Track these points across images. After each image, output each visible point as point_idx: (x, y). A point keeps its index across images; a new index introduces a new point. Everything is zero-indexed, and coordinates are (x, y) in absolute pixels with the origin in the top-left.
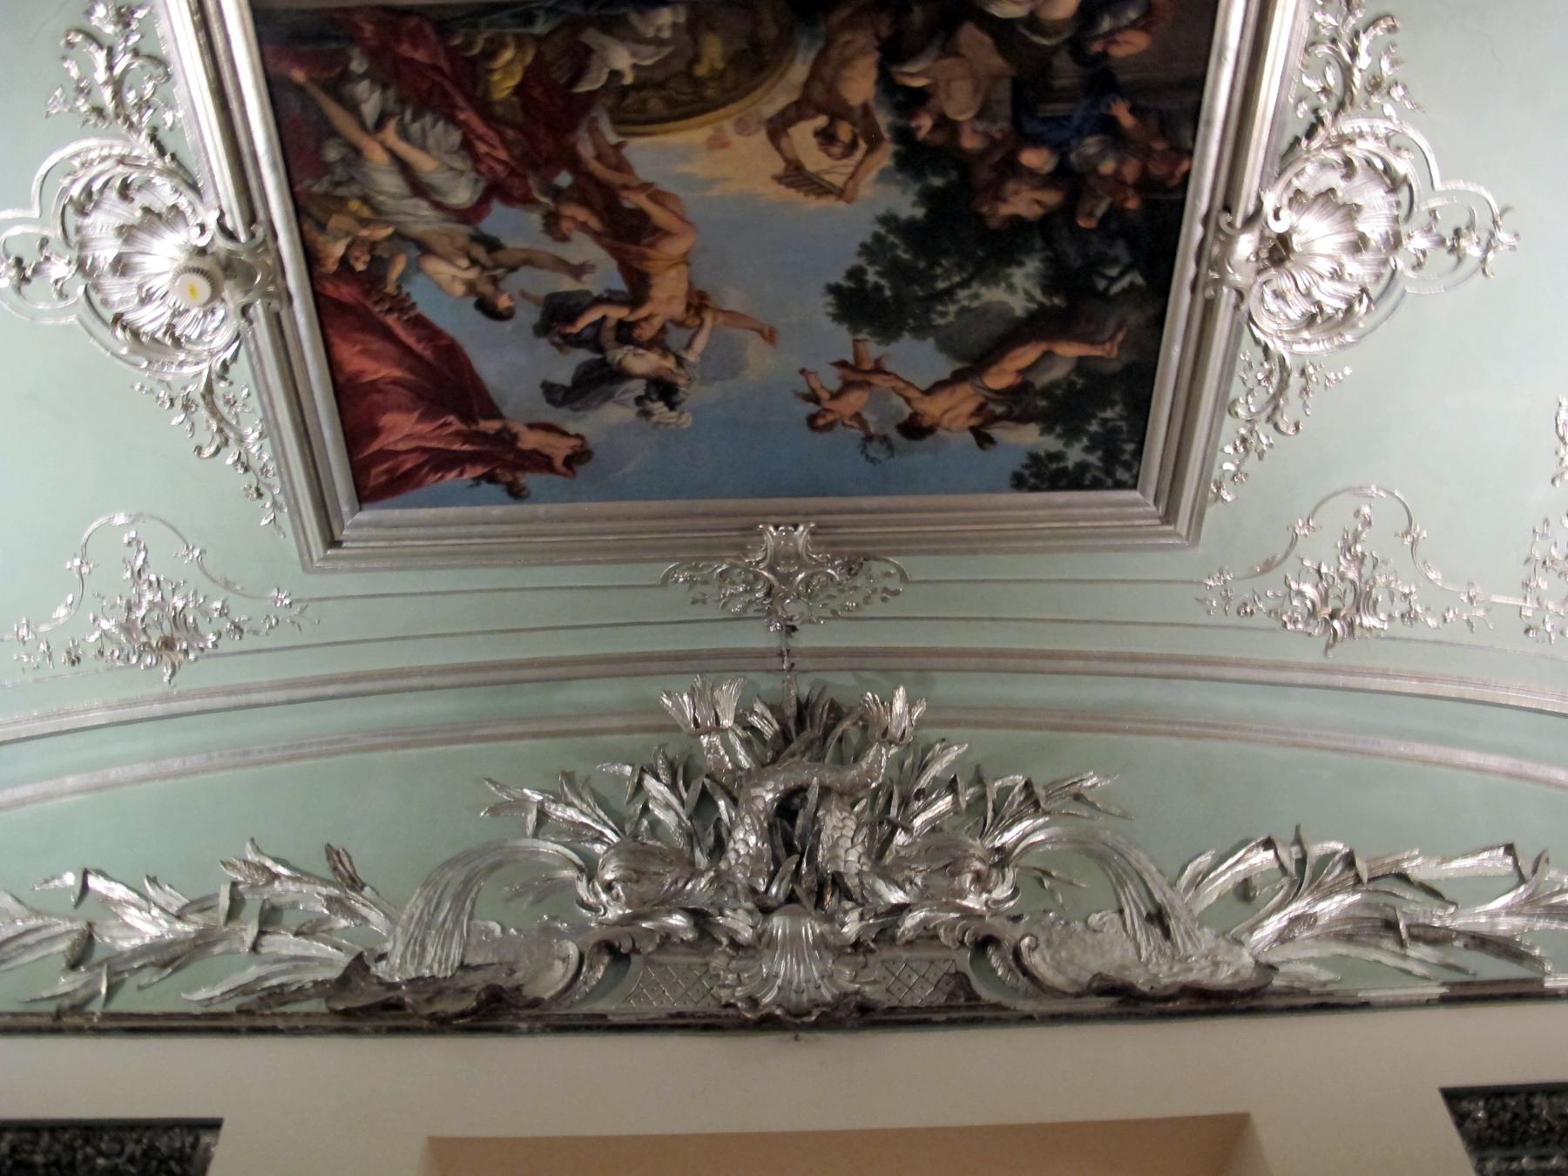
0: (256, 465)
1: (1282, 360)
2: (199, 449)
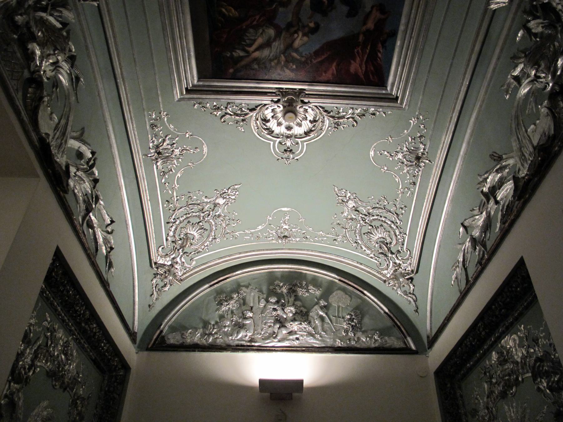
2: (353, 126)
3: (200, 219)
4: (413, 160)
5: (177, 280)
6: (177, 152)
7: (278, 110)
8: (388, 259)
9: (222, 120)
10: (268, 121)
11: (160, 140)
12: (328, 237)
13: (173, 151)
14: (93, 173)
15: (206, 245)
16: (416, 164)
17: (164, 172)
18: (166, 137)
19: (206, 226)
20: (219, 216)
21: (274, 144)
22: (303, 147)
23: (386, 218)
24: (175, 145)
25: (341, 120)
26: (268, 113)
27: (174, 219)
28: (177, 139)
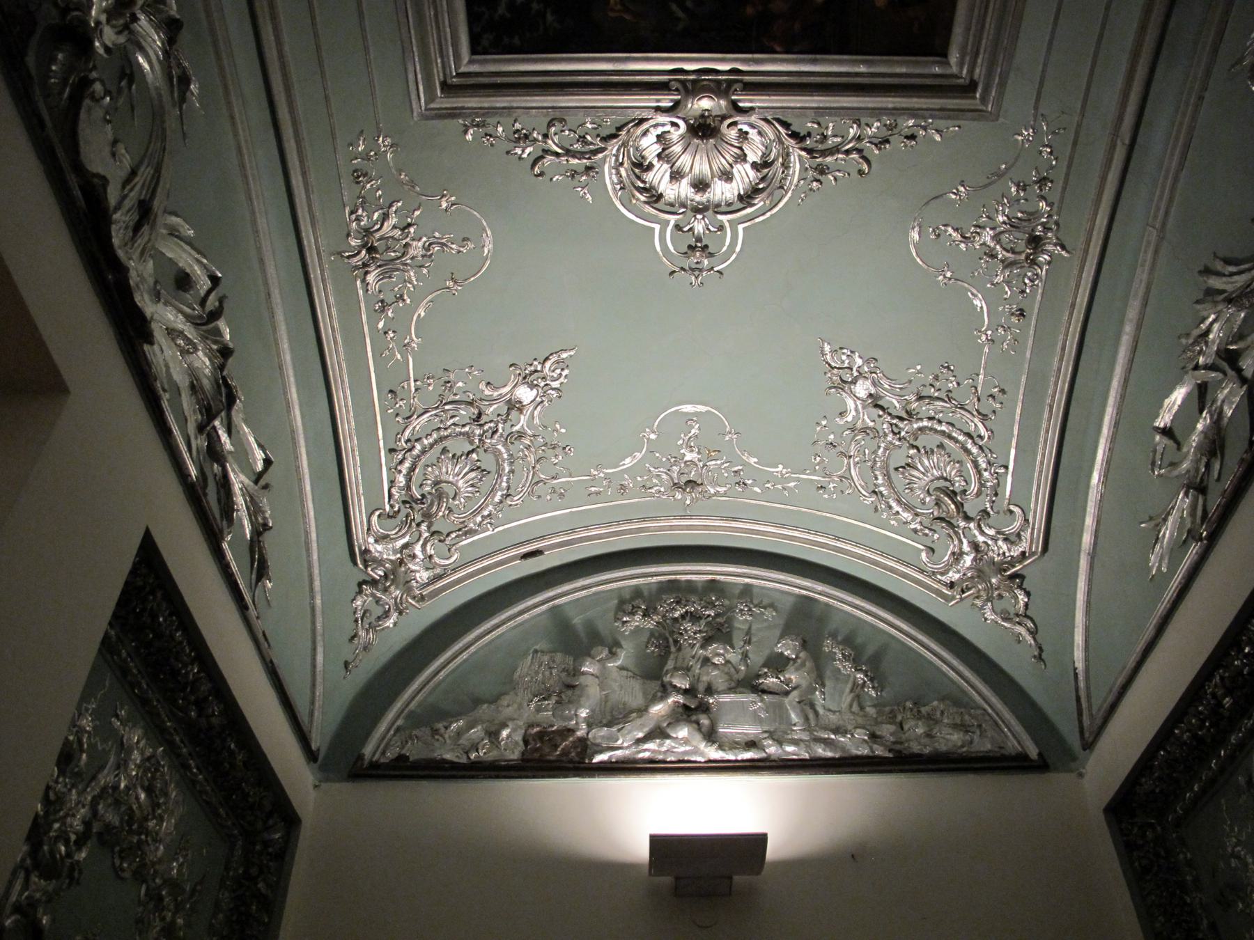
0: (885, 133)
1: (602, 150)
2: (861, 172)
3: (472, 443)
4: (1021, 245)
5: (414, 598)
6: (417, 248)
7: (675, 135)
8: (956, 533)
9: (537, 170)
10: (650, 167)
11: (376, 216)
12: (798, 480)
13: (407, 245)
14: (218, 333)
15: (486, 513)
16: (1027, 258)
17: (382, 301)
18: (391, 206)
19: (488, 462)
20: (521, 435)
21: (662, 236)
22: (735, 236)
23: (953, 425)
24: (412, 230)
25: (829, 159)
26: (650, 148)
27: (408, 441)
28: (417, 213)
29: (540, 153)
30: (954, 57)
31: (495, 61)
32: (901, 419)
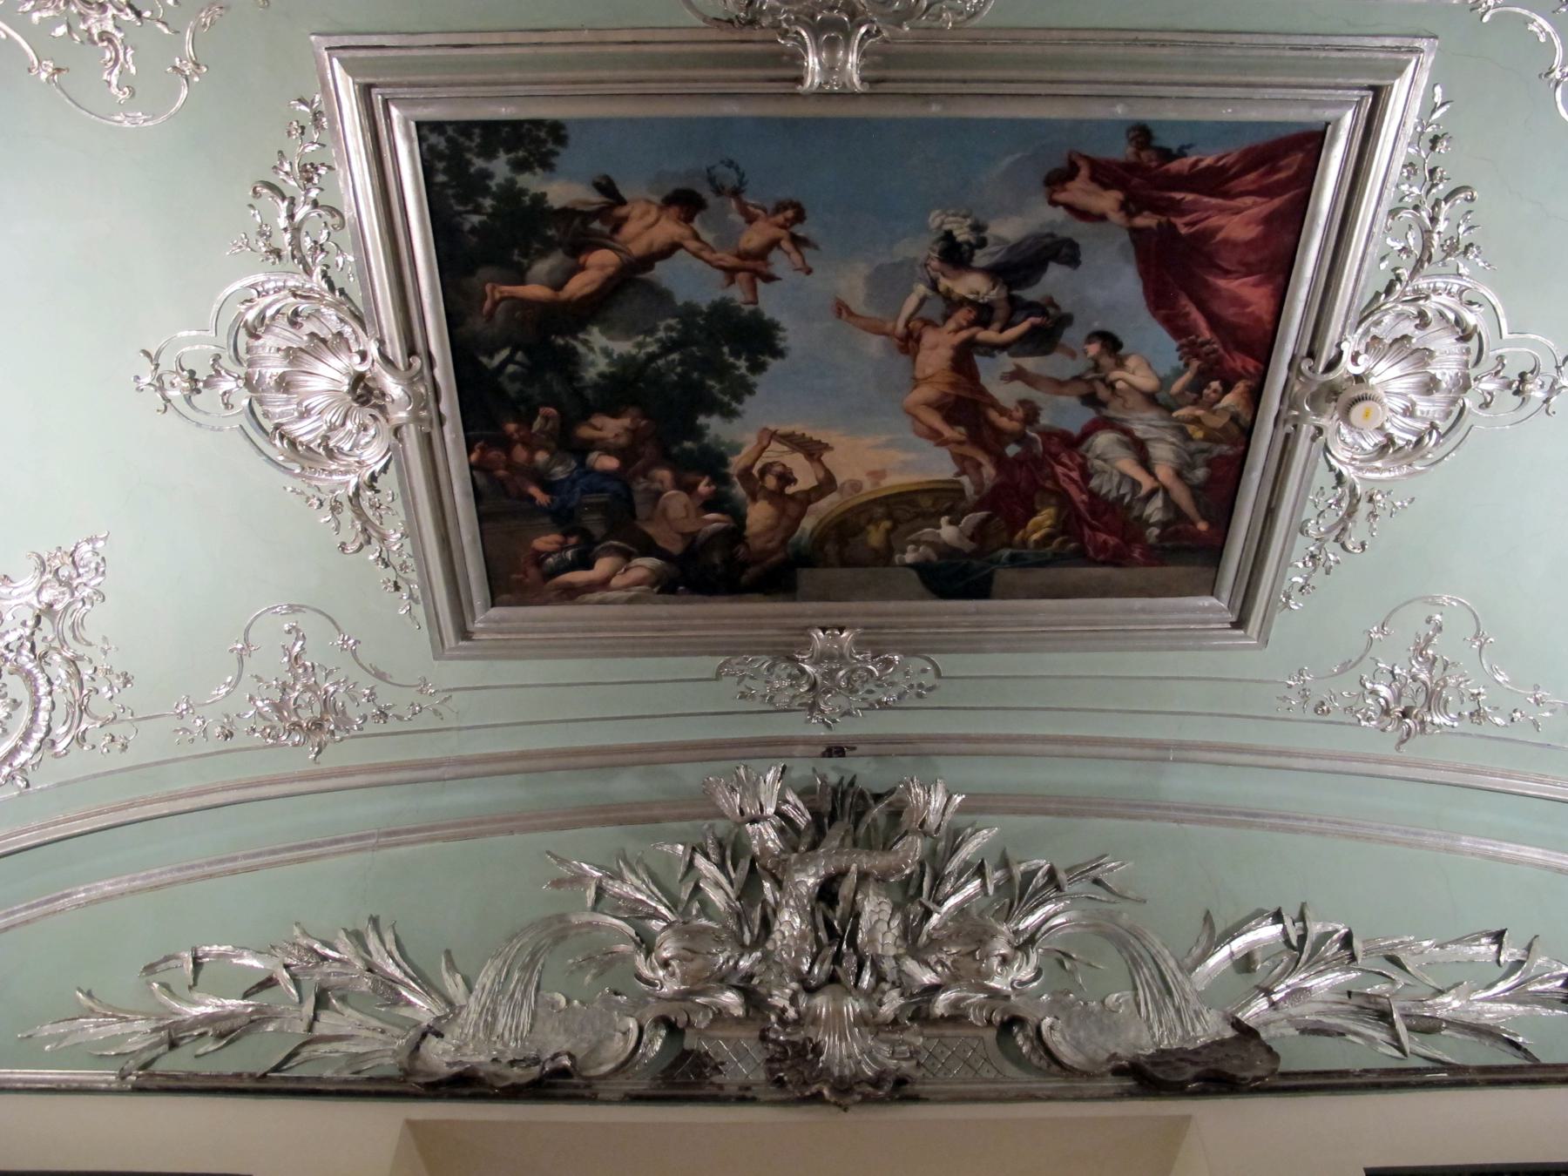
2: (343, 547)
29: (288, 195)
30: (495, 612)
31: (411, 152)
32: (33, 649)
